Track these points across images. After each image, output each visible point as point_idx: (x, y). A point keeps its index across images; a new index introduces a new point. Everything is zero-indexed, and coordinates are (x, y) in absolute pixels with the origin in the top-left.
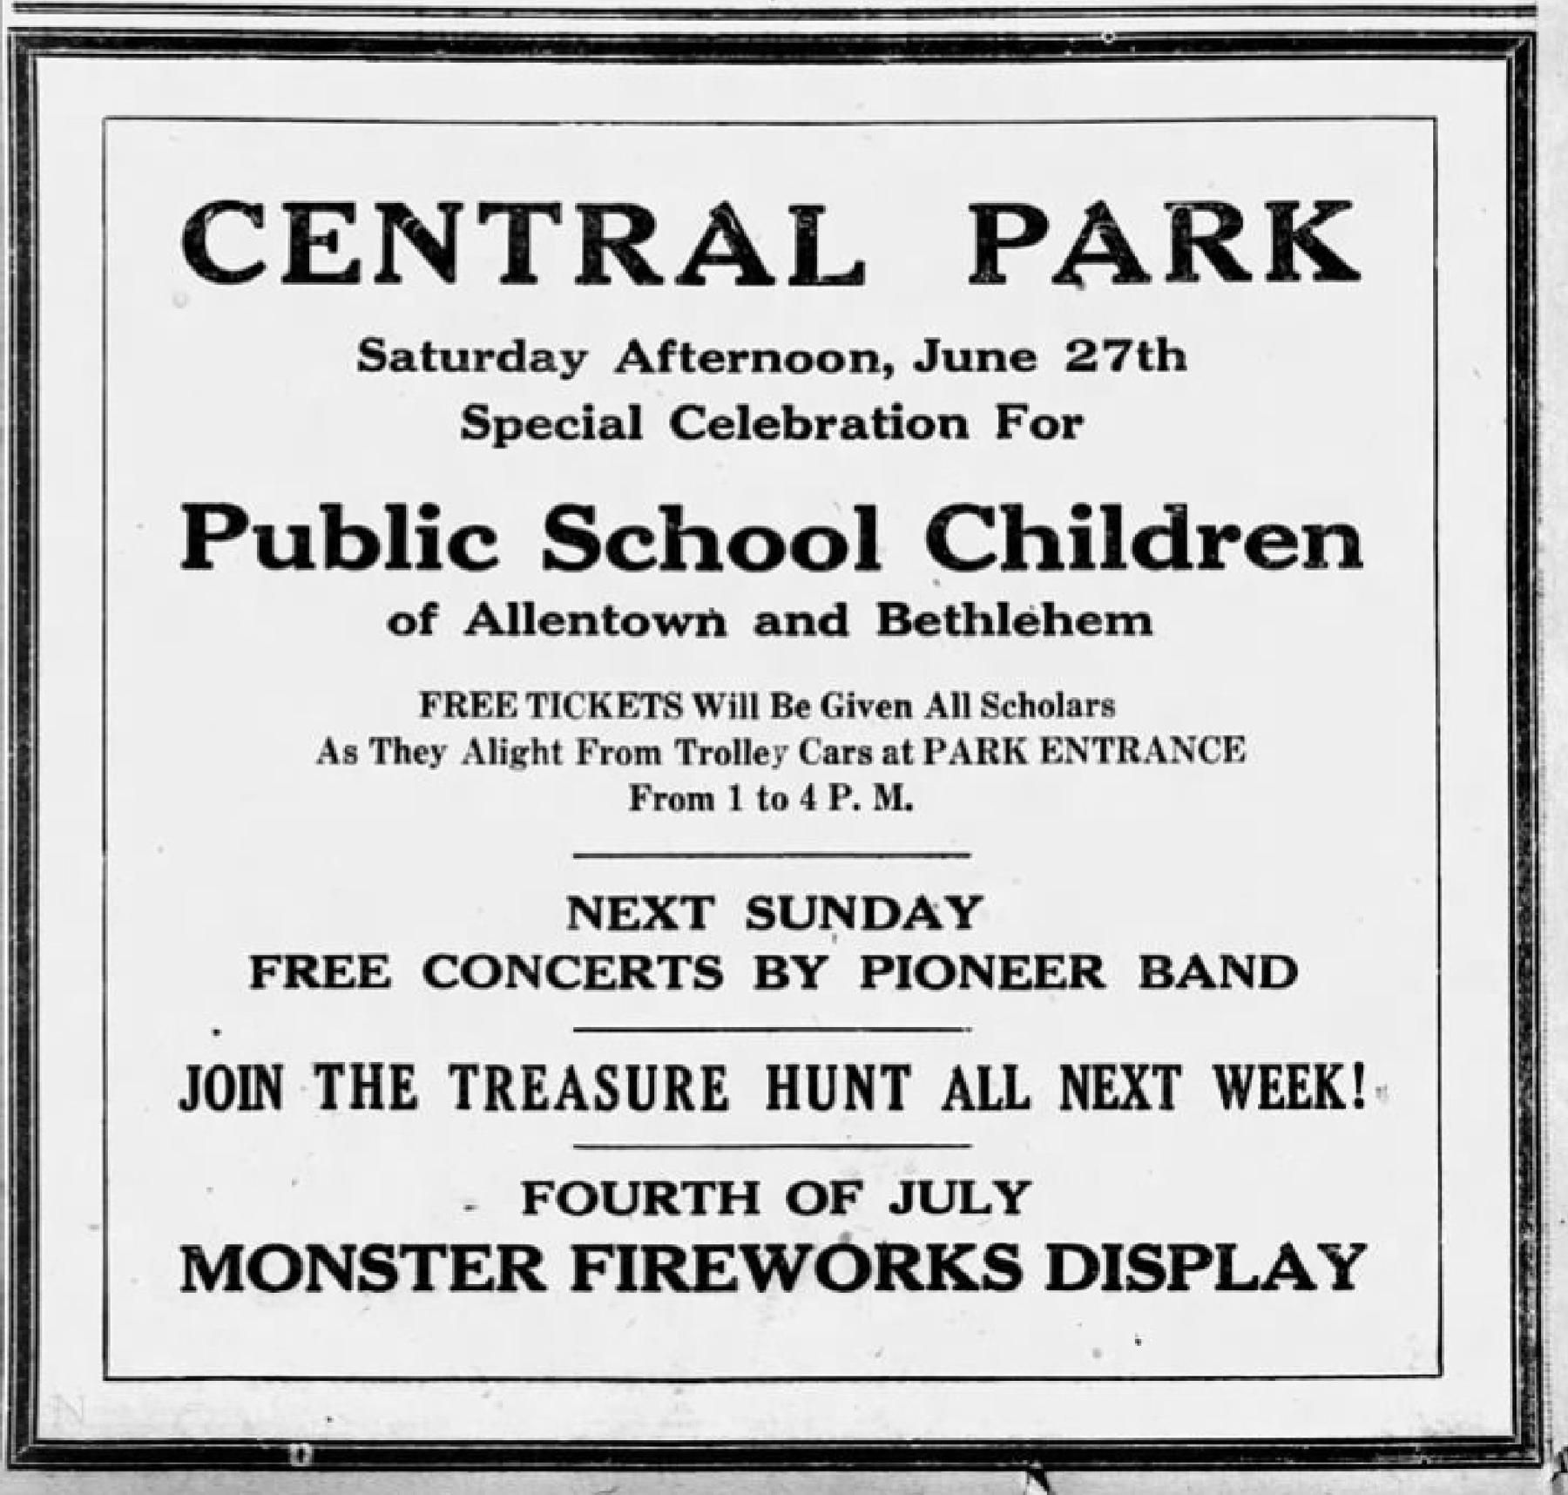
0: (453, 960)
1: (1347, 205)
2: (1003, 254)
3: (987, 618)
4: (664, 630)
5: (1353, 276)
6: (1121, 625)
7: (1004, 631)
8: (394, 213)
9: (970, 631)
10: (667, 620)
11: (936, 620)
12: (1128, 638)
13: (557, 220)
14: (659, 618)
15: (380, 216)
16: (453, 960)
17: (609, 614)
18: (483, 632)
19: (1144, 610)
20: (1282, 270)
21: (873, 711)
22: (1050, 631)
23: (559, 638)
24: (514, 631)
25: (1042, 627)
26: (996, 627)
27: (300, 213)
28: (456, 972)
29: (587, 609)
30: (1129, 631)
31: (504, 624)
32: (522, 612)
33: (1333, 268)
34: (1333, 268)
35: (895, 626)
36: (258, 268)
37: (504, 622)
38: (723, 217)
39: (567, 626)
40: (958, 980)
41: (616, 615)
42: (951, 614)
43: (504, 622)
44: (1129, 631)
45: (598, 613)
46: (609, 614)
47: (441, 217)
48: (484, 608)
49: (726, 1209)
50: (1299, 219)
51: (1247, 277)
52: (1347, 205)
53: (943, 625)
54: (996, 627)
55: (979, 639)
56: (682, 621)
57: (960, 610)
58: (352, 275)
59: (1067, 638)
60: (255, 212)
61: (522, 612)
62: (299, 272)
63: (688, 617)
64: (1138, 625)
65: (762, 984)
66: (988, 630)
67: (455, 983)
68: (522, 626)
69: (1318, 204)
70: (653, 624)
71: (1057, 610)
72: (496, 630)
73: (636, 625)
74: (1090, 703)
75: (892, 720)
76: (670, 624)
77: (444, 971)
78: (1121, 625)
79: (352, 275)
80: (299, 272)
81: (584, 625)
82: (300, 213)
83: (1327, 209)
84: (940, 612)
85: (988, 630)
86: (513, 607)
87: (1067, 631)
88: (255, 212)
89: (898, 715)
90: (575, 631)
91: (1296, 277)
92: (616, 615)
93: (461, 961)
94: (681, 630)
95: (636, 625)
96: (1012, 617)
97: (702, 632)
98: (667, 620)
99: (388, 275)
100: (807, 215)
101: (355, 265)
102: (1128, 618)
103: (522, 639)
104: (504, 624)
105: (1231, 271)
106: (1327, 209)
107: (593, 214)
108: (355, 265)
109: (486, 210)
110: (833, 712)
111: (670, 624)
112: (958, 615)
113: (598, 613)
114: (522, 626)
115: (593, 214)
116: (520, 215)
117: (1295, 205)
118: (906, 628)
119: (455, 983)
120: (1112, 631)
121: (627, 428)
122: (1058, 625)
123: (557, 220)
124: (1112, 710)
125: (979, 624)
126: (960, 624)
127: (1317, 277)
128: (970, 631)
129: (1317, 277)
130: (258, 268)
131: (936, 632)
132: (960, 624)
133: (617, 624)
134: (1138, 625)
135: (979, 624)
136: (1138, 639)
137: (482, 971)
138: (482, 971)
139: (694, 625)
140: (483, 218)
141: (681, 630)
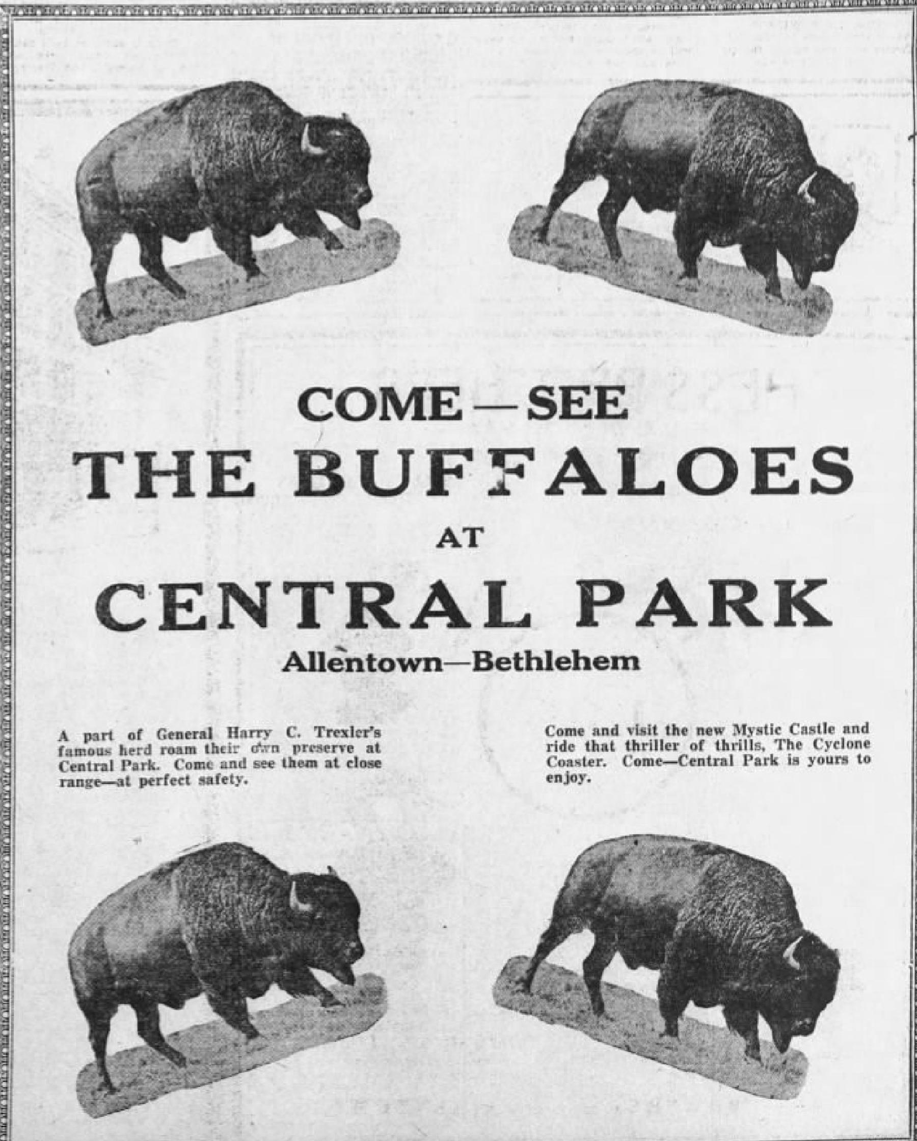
0: (328, 393)
1: (824, 582)
2: (597, 610)
3: (539, 661)
4: (404, 669)
5: (829, 623)
6: (620, 663)
7: (549, 668)
8: (231, 590)
9: (529, 668)
10: (406, 662)
11: (508, 661)
12: (625, 672)
13: (331, 591)
14: (401, 661)
15: (220, 590)
16: (328, 393)
17: (370, 658)
18: (294, 669)
19: (635, 654)
20: (785, 620)
21: (346, 750)
22: (577, 667)
23: (339, 673)
24: (312, 669)
25: (572, 665)
26: (544, 665)
27: (170, 590)
28: (330, 406)
29: (357, 656)
30: (626, 667)
31: (307, 664)
32: (317, 658)
33: (815, 619)
34: (815, 619)
35: (483, 665)
36: (142, 622)
37: (306, 663)
38: (665, 589)
39: (345, 666)
40: (379, 412)
41: (375, 660)
42: (517, 657)
43: (306, 663)
44: (626, 667)
45: (364, 659)
46: (370, 658)
47: (257, 591)
48: (294, 655)
49: (146, 491)
50: (795, 590)
51: (759, 623)
52: (824, 582)
53: (512, 665)
54: (544, 665)
55: (534, 673)
56: (415, 663)
57: (523, 655)
58: (201, 624)
59: (587, 672)
60: (140, 591)
61: (317, 658)
62: (170, 623)
63: (419, 660)
64: (631, 663)
65: (305, 490)
66: (540, 668)
67: (330, 415)
68: (317, 666)
69: (807, 582)
70: (398, 665)
71: (581, 654)
72: (302, 668)
73: (387, 665)
74: (251, 732)
75: (354, 769)
76: (409, 665)
77: (318, 404)
78: (620, 663)
79: (201, 624)
80: (170, 623)
81: (355, 666)
82: (170, 590)
83: (812, 585)
84: (511, 657)
85: (540, 668)
86: (312, 654)
87: (587, 667)
88: (140, 591)
89: (699, 765)
90: (350, 669)
91: (793, 624)
92: (375, 660)
93: (336, 394)
94: (414, 669)
95: (387, 665)
96: (554, 659)
97: (427, 669)
98: (406, 662)
99: (226, 624)
100: (495, 590)
101: (796, 484)
102: (625, 660)
103: (317, 675)
104: (307, 664)
105: (750, 620)
106: (812, 585)
107: (356, 589)
108: (796, 484)
109: (288, 587)
110: (162, 737)
111: (409, 665)
112: (522, 659)
113: (364, 659)
114: (317, 666)
115: (356, 589)
116: (309, 589)
117: (793, 582)
118: (490, 667)
119: (330, 415)
120: (615, 667)
121: (729, 762)
122: (582, 663)
123: (331, 591)
124: (847, 761)
125: (534, 664)
126: (523, 664)
127: (806, 624)
128: (529, 668)
129: (806, 624)
130: (142, 622)
131: (509, 669)
132: (523, 664)
133: (375, 665)
134: (631, 663)
135: (534, 664)
136: (631, 673)
137: (356, 405)
138: (356, 405)
139: (422, 665)
140: (286, 591)
141: (414, 669)
